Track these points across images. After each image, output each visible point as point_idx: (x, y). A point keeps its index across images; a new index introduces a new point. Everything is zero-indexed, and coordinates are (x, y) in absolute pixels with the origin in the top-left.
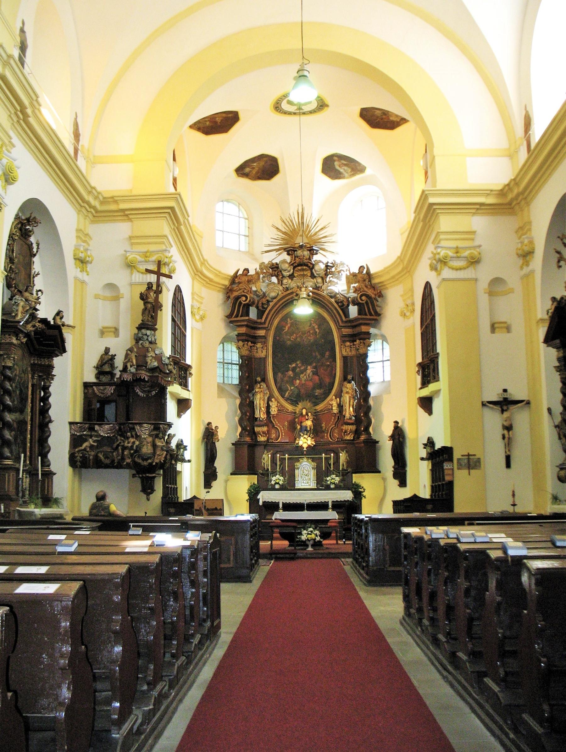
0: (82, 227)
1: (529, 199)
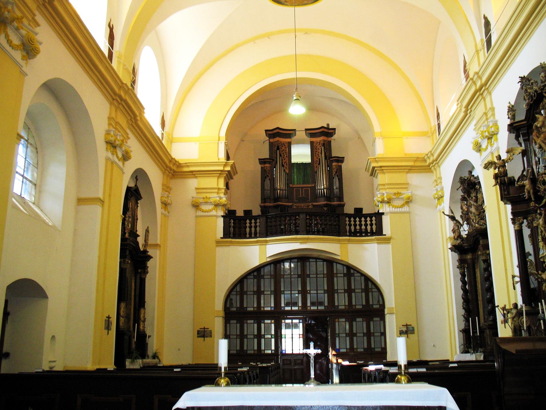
0: (113, 115)
1: (439, 164)
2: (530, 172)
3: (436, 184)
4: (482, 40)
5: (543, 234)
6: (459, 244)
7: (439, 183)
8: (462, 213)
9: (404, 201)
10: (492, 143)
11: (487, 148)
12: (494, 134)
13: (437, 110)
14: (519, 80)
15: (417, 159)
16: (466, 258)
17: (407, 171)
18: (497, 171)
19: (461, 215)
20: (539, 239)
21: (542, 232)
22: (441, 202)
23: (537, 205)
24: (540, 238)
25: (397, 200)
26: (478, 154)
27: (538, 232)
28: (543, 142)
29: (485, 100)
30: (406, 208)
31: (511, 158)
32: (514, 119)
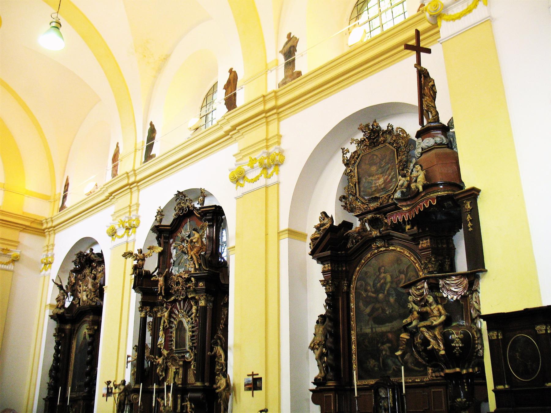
1: (56, 231)
2: (167, 271)
3: (46, 249)
4: (143, 142)
5: (165, 325)
6: (61, 313)
7: (50, 249)
8: (68, 283)
9: (11, 259)
10: (130, 234)
11: (123, 236)
12: (134, 227)
13: (67, 180)
14: (176, 193)
15: (34, 221)
16: (65, 327)
17: (21, 229)
18: (135, 262)
19: (67, 286)
20: (160, 329)
21: (164, 322)
22: (48, 268)
23: (165, 300)
24: (161, 328)
25: (3, 256)
26: (110, 238)
27: (161, 322)
28: (195, 255)
29: (131, 194)
30: (11, 266)
31: (150, 255)
32: (161, 220)
